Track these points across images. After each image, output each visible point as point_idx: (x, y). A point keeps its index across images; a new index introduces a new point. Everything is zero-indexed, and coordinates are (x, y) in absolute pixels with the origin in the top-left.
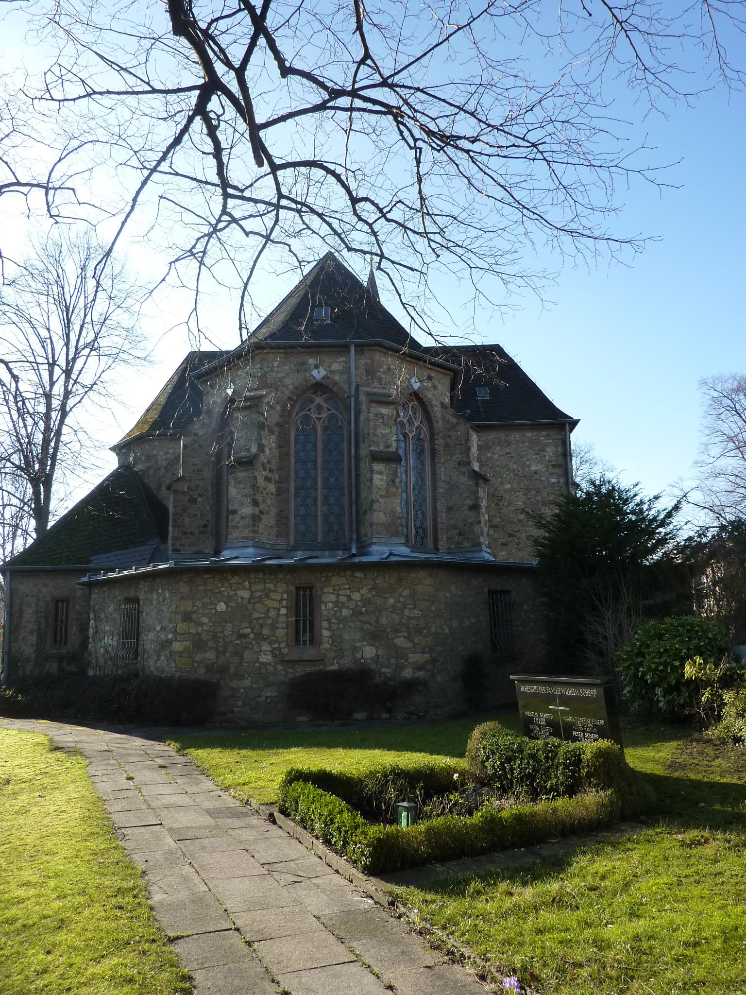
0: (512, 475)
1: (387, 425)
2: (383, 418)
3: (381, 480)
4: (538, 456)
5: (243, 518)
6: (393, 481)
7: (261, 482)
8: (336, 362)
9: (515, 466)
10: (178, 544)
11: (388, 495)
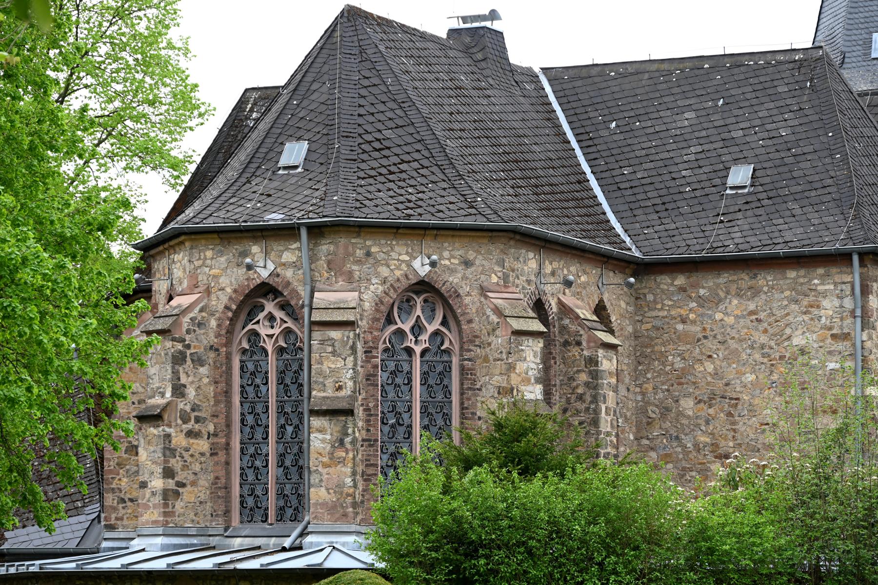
0: (757, 356)
1: (339, 355)
2: (333, 345)
3: (323, 441)
4: (806, 318)
5: (153, 494)
6: (342, 443)
7: (179, 440)
8: (287, 249)
9: (763, 339)
10: (113, 516)
11: (334, 461)
